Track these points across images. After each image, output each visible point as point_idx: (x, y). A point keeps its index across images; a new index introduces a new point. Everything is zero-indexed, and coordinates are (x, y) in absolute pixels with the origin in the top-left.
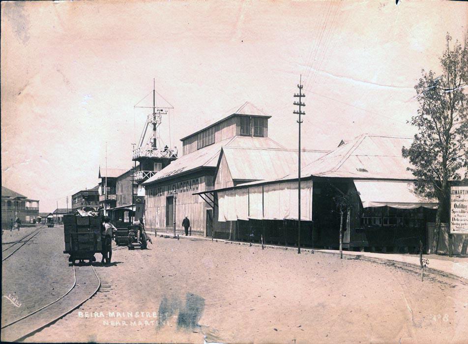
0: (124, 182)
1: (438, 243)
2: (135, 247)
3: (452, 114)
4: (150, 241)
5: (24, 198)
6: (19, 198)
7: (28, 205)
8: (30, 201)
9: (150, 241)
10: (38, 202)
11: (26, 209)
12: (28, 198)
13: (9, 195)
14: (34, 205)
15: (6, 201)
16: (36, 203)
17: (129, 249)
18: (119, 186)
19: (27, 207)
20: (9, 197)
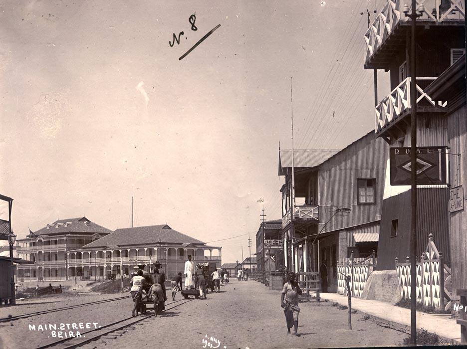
0: (336, 171)
1: (141, 296)
2: (288, 198)
3: (347, 243)
4: (376, 251)
5: (203, 244)
6: (194, 245)
7: (207, 253)
8: (211, 249)
9: (376, 251)
10: (220, 249)
11: (205, 259)
12: (207, 245)
13: (181, 242)
14: (215, 253)
15: (176, 249)
16: (217, 250)
17: (375, 179)
18: (323, 184)
19: (206, 257)
20: (181, 244)
